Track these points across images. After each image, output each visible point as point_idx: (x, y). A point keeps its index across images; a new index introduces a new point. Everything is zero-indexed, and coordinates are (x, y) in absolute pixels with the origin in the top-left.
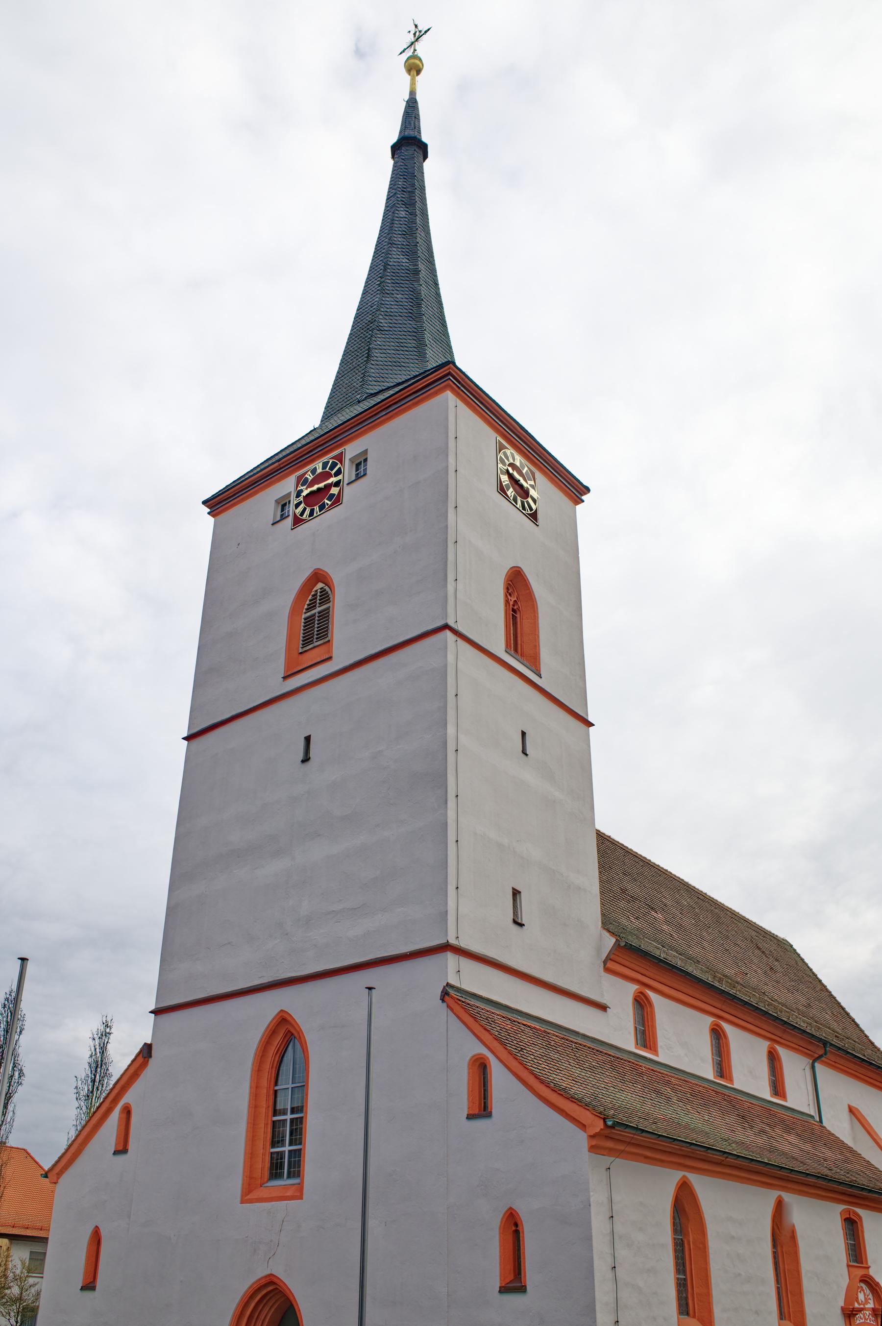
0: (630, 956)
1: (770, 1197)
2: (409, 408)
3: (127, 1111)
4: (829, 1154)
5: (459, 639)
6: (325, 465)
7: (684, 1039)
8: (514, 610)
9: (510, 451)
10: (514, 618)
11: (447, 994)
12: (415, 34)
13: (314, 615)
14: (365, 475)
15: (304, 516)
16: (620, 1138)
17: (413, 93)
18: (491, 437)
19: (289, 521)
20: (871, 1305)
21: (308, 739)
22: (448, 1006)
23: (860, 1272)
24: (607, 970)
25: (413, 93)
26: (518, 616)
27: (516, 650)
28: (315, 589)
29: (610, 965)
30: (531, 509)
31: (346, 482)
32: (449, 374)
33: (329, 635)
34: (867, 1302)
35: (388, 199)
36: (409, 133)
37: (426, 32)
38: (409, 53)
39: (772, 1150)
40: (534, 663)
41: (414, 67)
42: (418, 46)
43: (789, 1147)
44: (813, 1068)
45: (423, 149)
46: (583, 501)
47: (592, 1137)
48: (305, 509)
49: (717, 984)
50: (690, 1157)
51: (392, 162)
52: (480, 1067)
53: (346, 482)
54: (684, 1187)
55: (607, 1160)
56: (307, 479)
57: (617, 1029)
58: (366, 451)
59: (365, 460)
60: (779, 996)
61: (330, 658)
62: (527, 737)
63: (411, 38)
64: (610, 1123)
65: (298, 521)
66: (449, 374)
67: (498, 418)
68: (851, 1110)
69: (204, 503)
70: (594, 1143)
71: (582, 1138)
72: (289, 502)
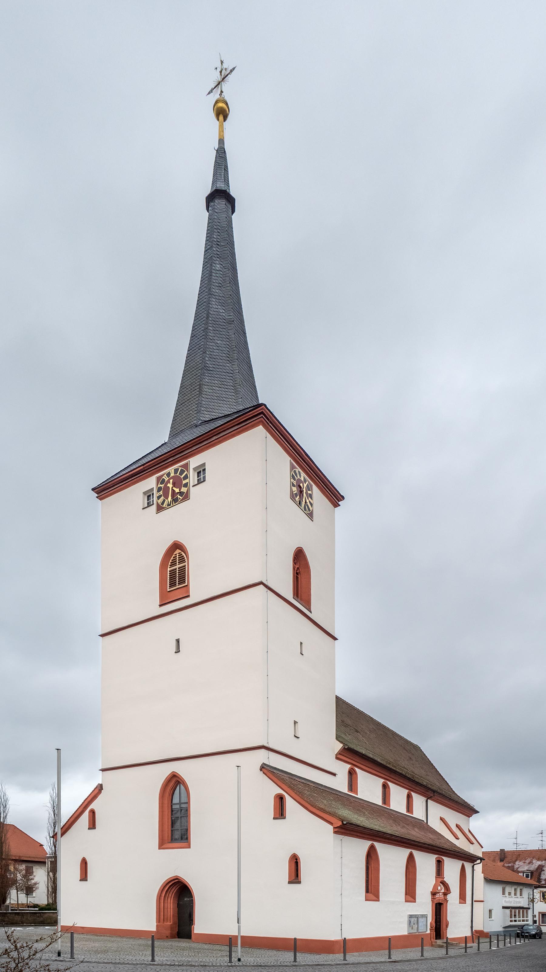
0: (348, 754)
1: (405, 852)
2: (234, 436)
3: (93, 812)
4: (431, 836)
5: (268, 591)
6: (176, 471)
7: (369, 788)
8: (297, 573)
9: (298, 469)
10: (297, 578)
11: (265, 768)
12: (221, 72)
13: (176, 569)
14: (204, 481)
15: (164, 505)
16: (346, 829)
17: (221, 141)
18: (286, 460)
19: (154, 507)
20: (443, 891)
21: (178, 641)
22: (264, 773)
23: (441, 880)
24: (337, 758)
25: (221, 141)
26: (299, 576)
27: (297, 596)
28: (175, 553)
29: (339, 756)
30: (309, 510)
31: (191, 484)
32: (262, 413)
33: (186, 582)
34: (441, 890)
35: (206, 251)
36: (221, 186)
37: (231, 71)
38: (216, 96)
39: (409, 834)
40: (307, 604)
41: (222, 113)
42: (225, 86)
43: (415, 834)
44: (427, 801)
45: (231, 201)
46: (339, 505)
47: (334, 828)
48: (164, 501)
49: (388, 766)
50: (376, 836)
51: (206, 215)
52: (280, 799)
53: (191, 484)
54: (372, 848)
55: (341, 837)
56: (164, 480)
57: (340, 784)
58: (204, 464)
59: (204, 470)
60: (417, 771)
61: (188, 596)
62: (303, 645)
63: (217, 77)
64: (345, 823)
65: (160, 509)
66: (262, 413)
67: (291, 446)
68: (441, 819)
69: (93, 489)
70: (336, 830)
71: (331, 828)
72: (153, 494)
